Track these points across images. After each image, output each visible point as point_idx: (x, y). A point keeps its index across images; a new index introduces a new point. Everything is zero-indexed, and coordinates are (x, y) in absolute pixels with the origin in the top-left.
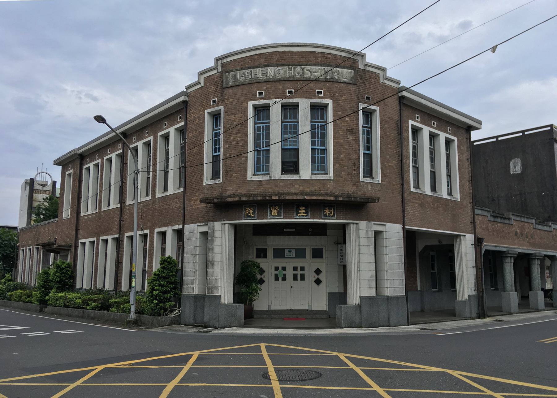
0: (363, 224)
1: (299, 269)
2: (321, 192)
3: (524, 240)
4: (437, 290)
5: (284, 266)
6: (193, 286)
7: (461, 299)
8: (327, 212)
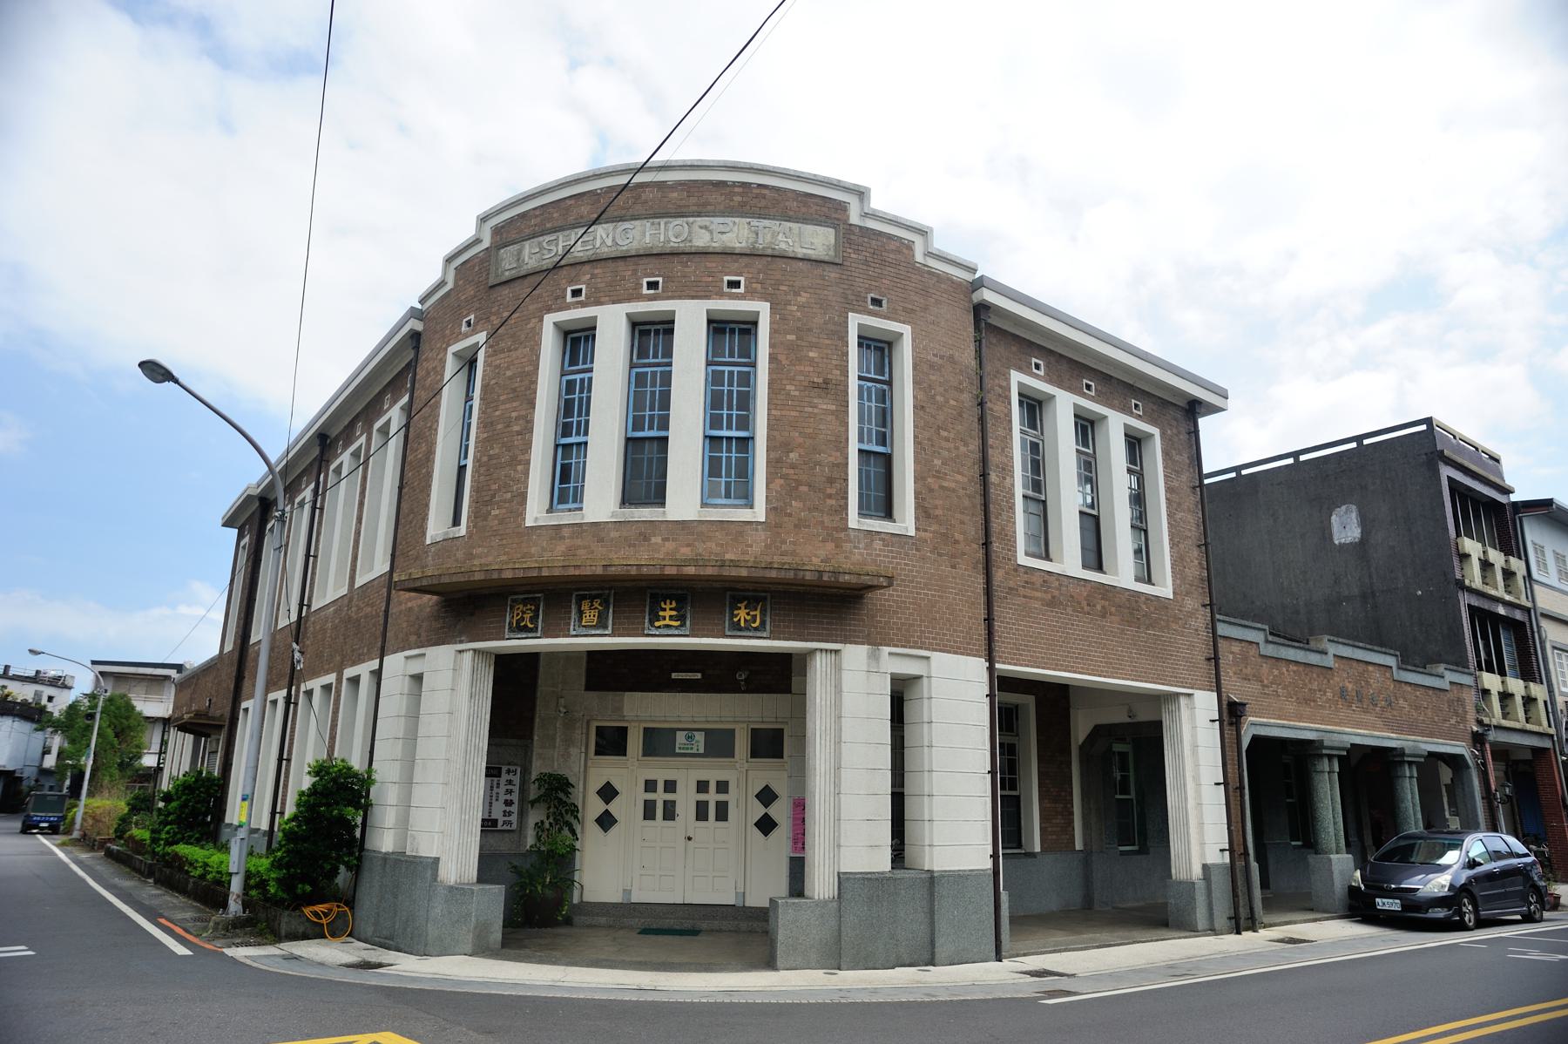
0: (855, 655)
1: (713, 787)
2: (728, 556)
3: (1366, 711)
4: (1135, 848)
8: (742, 614)
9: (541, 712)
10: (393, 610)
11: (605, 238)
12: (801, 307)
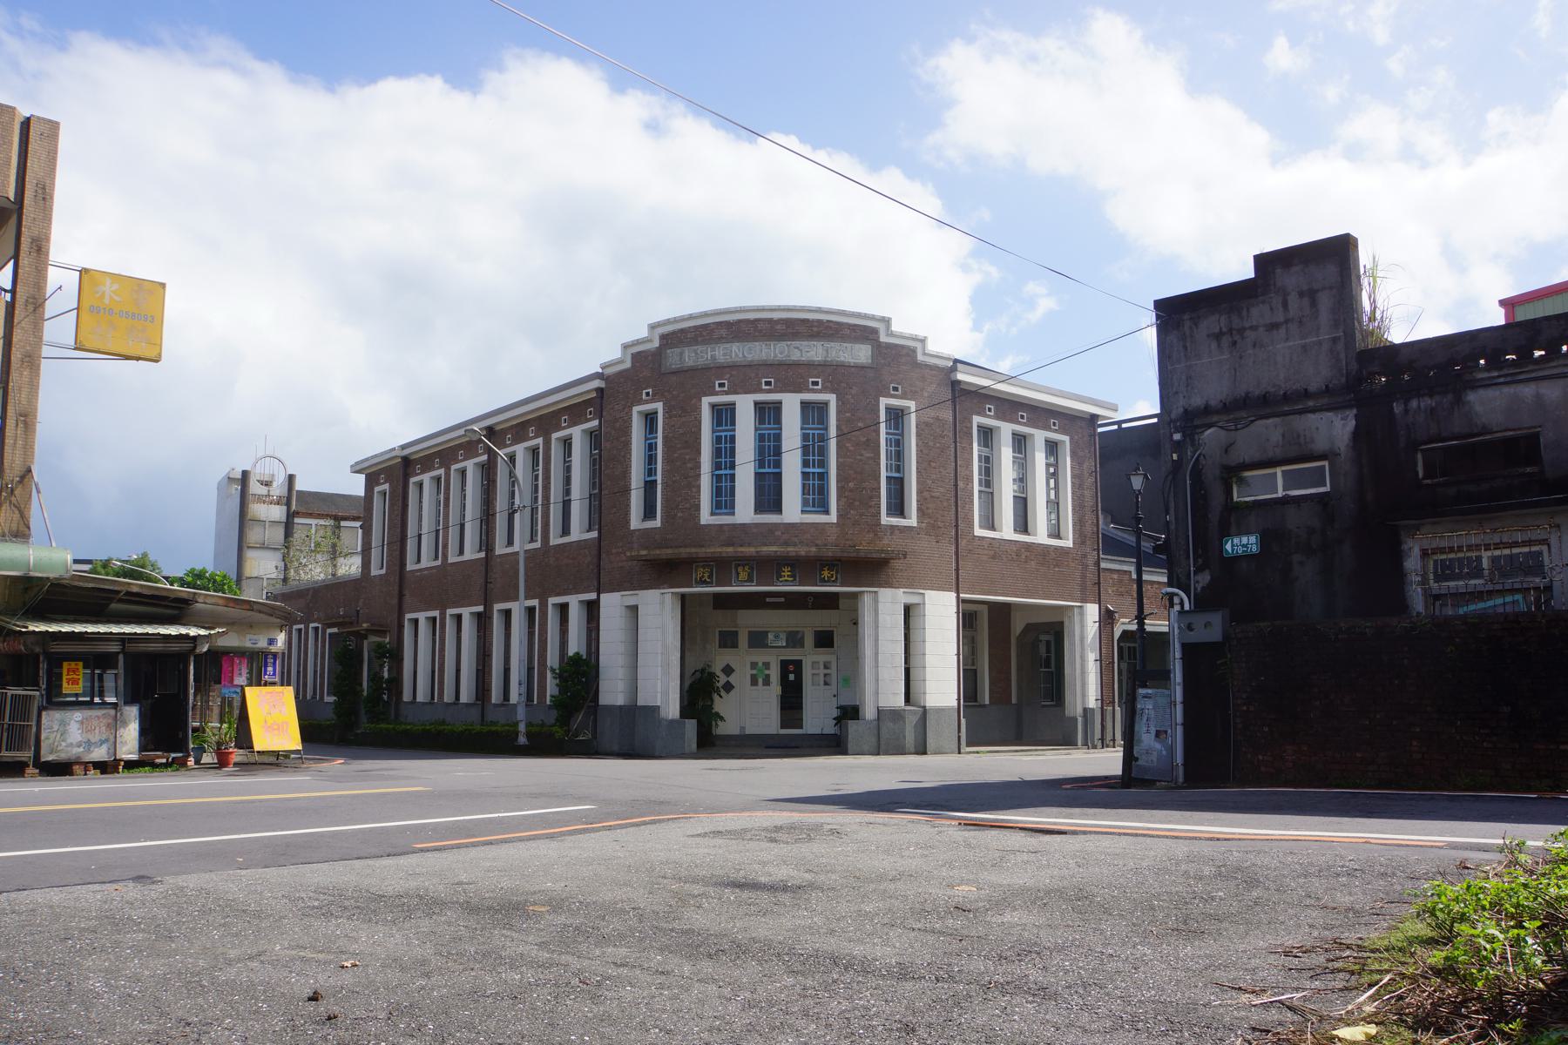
0: (885, 594)
6: (612, 692)
8: (826, 574)
11: (737, 352)
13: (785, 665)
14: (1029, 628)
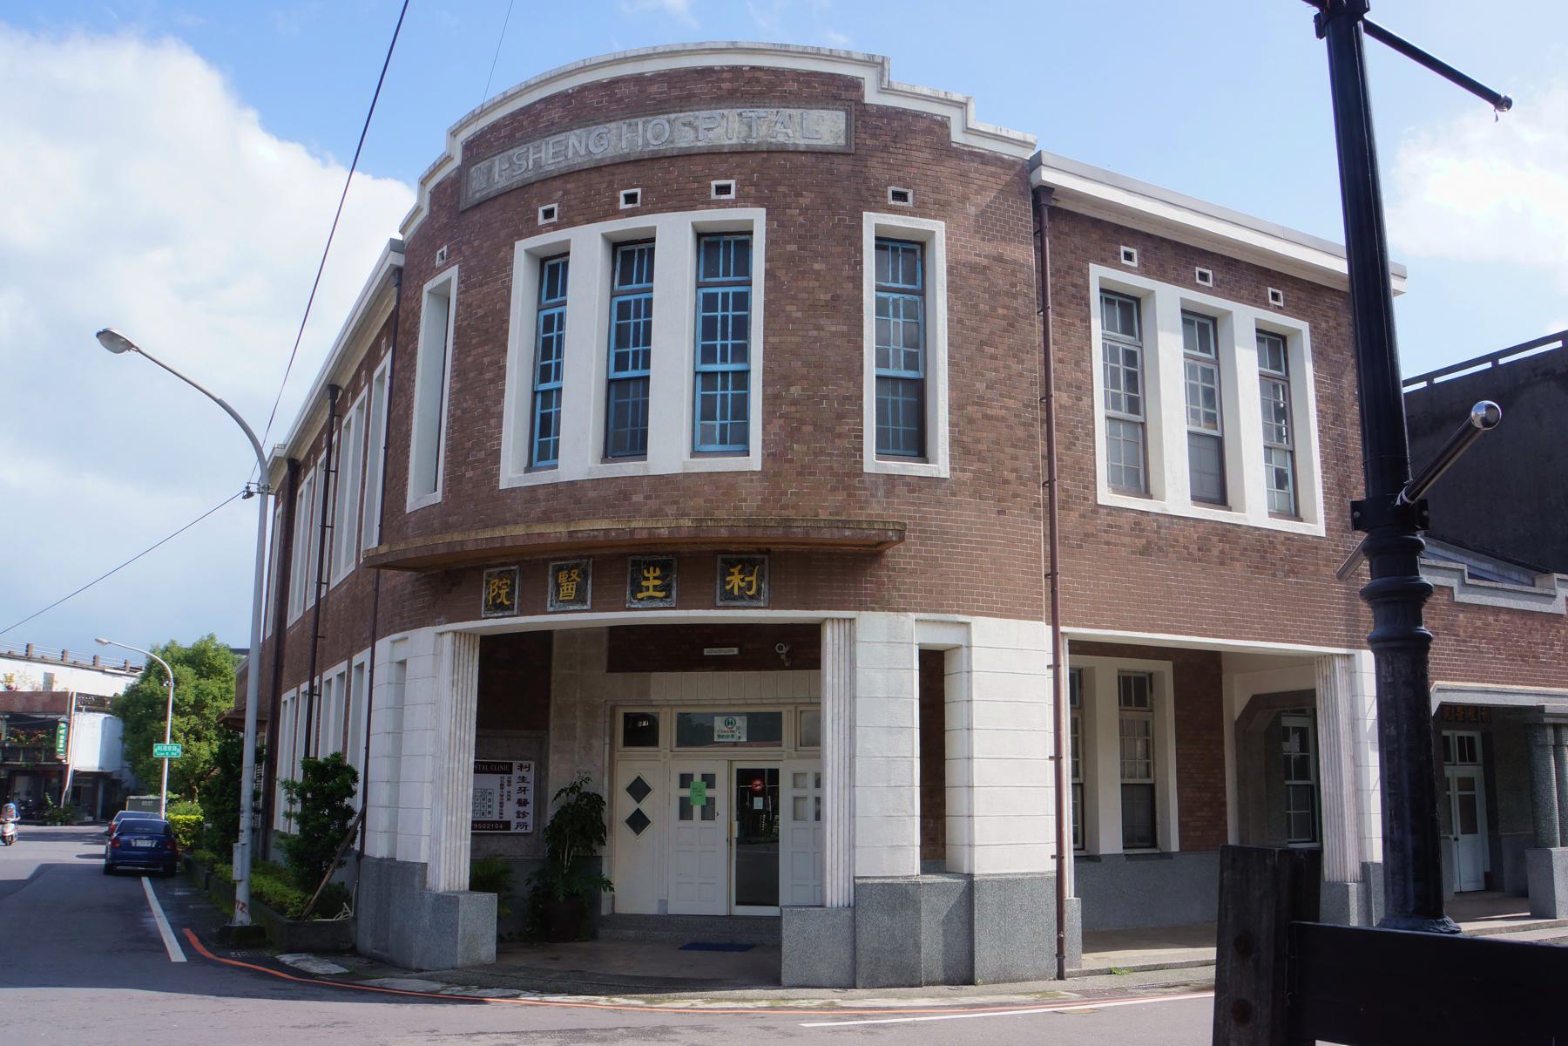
0: (873, 625)
5: (709, 771)
7: (1337, 877)
8: (736, 581)
9: (556, 700)
10: (382, 589)
12: (804, 211)
13: (745, 777)
14: (1258, 703)
